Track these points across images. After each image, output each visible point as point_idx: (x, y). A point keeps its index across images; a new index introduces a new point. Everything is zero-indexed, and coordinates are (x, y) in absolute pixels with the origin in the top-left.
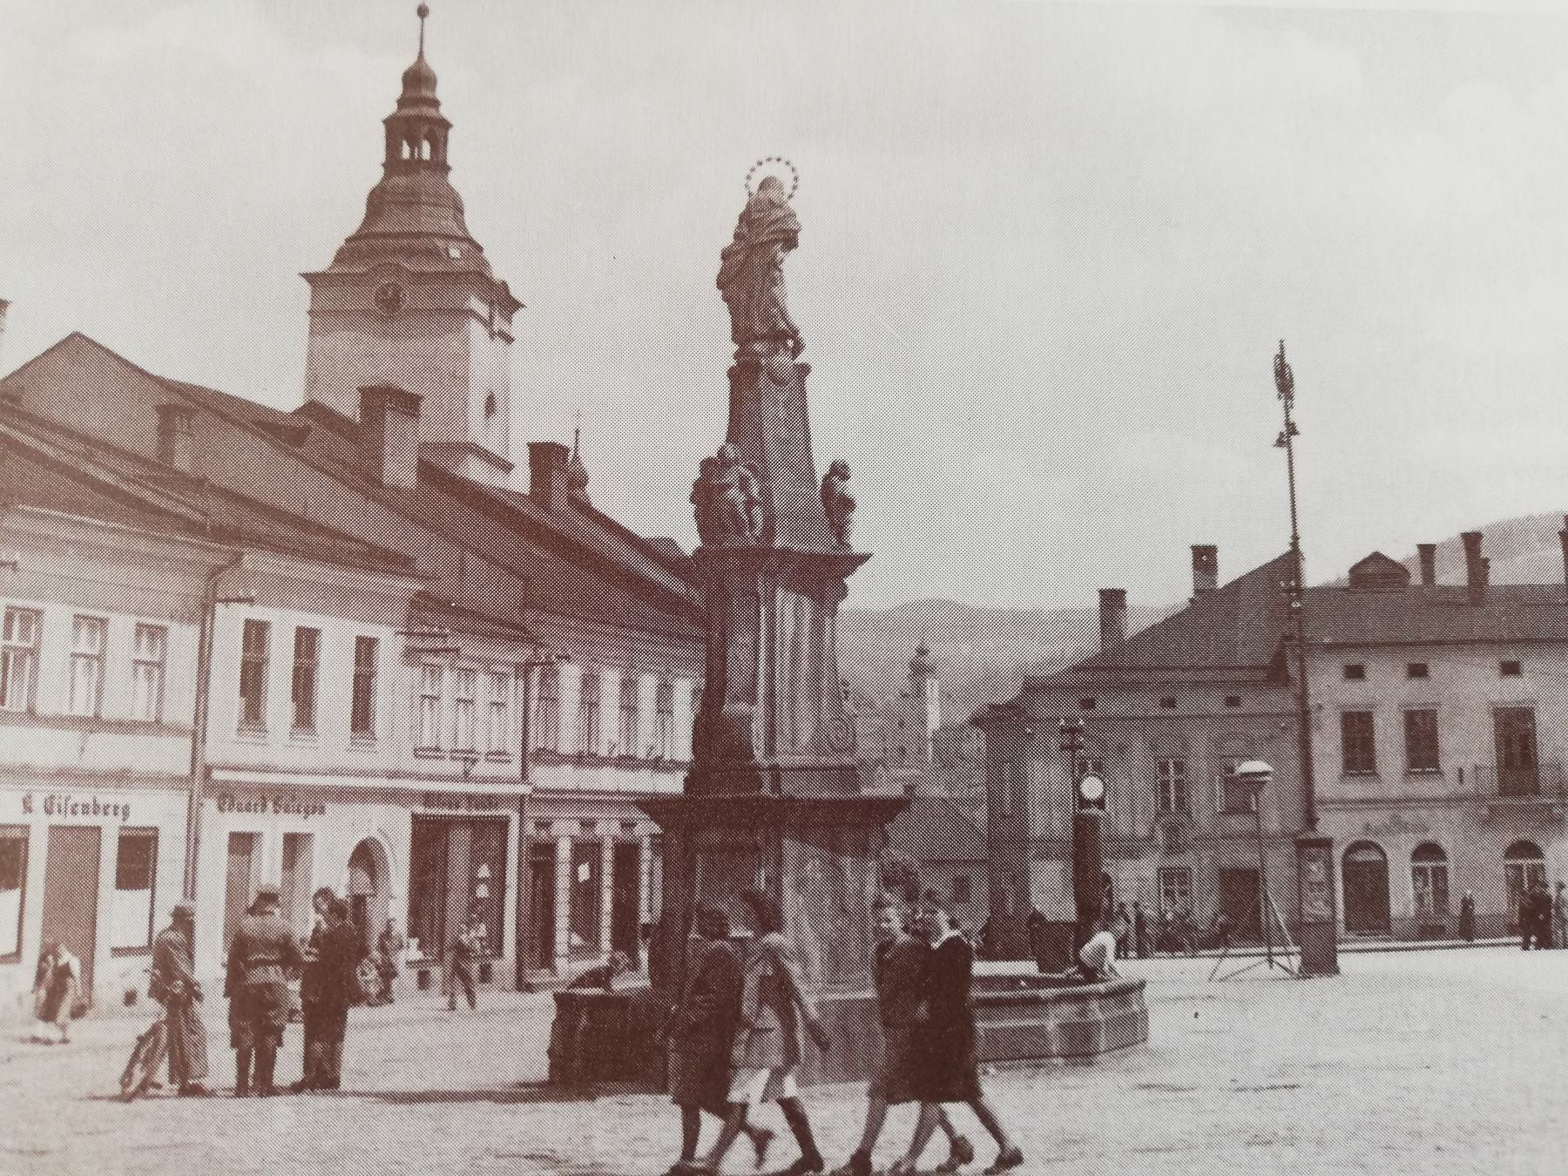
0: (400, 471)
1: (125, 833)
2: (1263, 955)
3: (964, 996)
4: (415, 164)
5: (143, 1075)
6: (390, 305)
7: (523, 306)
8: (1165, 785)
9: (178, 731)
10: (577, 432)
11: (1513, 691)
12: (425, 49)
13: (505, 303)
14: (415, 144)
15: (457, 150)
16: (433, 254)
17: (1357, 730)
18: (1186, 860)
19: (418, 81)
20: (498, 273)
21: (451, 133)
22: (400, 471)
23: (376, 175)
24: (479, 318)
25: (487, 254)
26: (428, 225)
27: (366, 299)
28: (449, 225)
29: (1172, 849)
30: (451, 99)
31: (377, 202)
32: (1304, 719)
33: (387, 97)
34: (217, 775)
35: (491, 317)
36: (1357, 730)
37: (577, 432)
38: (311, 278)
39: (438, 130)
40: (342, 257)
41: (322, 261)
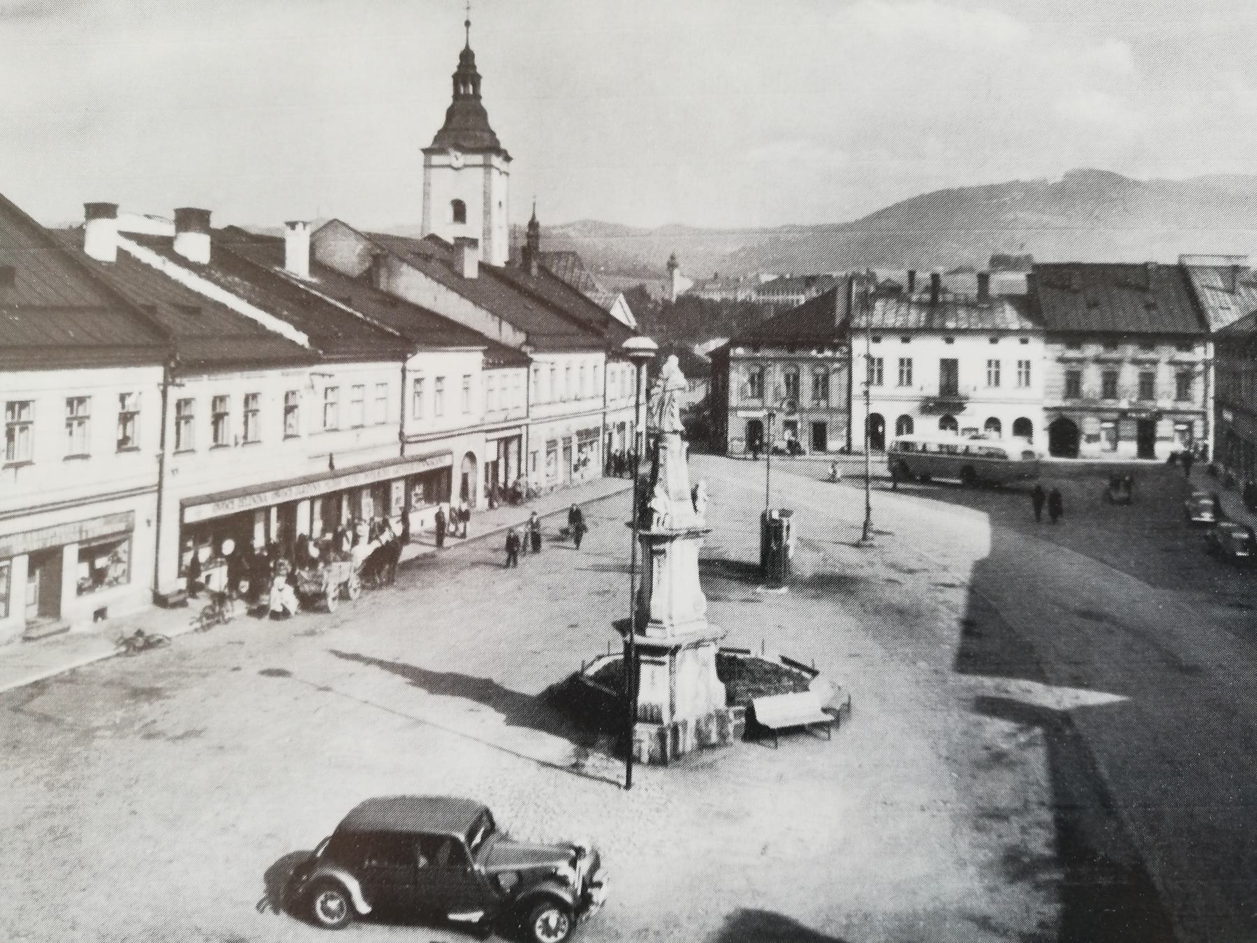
0: (471, 271)
2: (860, 462)
4: (466, 96)
5: (962, 313)
8: (872, 371)
11: (949, 352)
14: (465, 85)
15: (484, 90)
17: (875, 365)
18: (796, 417)
19: (467, 57)
22: (471, 271)
23: (449, 101)
25: (498, 136)
29: (790, 413)
30: (481, 65)
33: (453, 64)
36: (875, 365)
39: (476, 80)
40: (436, 139)
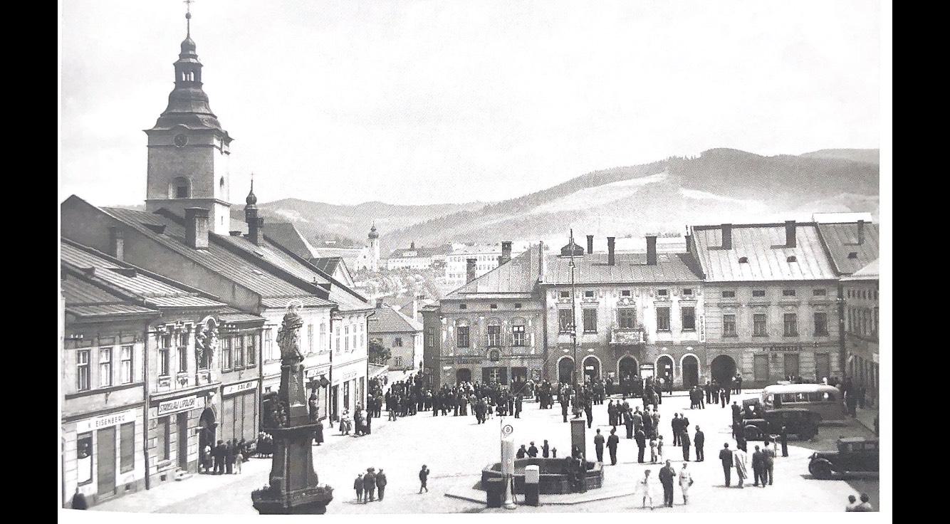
1: (81, 437)
3: (680, 420)
6: (180, 141)
7: (474, 488)
9: (138, 385)
10: (252, 181)
12: (190, 32)
13: (226, 139)
16: (199, 122)
19: (188, 47)
20: (224, 128)
21: (202, 68)
24: (217, 147)
26: (194, 111)
27: (171, 141)
28: (203, 110)
31: (173, 97)
32: (544, 312)
34: (153, 399)
35: (221, 146)
37: (252, 181)
38: (148, 132)
39: (197, 68)
40: (159, 122)
41: (151, 124)
